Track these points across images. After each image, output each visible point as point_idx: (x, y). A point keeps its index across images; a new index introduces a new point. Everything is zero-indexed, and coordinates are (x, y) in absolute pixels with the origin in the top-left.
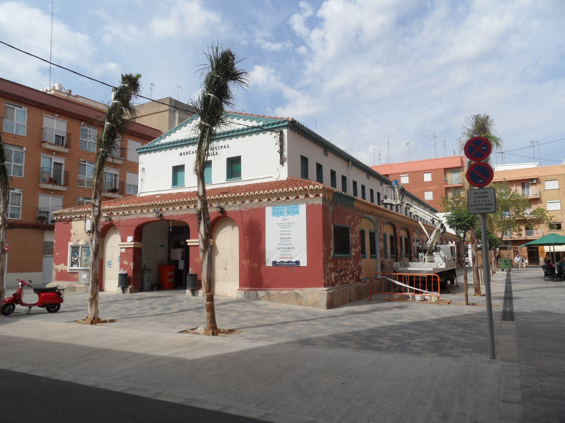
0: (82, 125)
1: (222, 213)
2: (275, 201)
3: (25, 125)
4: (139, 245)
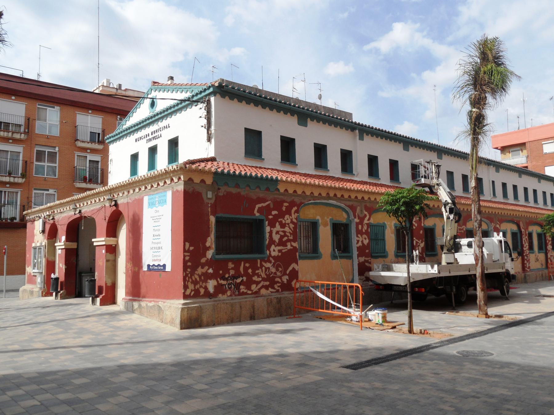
0: (118, 119)
1: (116, 207)
2: (150, 188)
3: (58, 125)
4: (73, 245)
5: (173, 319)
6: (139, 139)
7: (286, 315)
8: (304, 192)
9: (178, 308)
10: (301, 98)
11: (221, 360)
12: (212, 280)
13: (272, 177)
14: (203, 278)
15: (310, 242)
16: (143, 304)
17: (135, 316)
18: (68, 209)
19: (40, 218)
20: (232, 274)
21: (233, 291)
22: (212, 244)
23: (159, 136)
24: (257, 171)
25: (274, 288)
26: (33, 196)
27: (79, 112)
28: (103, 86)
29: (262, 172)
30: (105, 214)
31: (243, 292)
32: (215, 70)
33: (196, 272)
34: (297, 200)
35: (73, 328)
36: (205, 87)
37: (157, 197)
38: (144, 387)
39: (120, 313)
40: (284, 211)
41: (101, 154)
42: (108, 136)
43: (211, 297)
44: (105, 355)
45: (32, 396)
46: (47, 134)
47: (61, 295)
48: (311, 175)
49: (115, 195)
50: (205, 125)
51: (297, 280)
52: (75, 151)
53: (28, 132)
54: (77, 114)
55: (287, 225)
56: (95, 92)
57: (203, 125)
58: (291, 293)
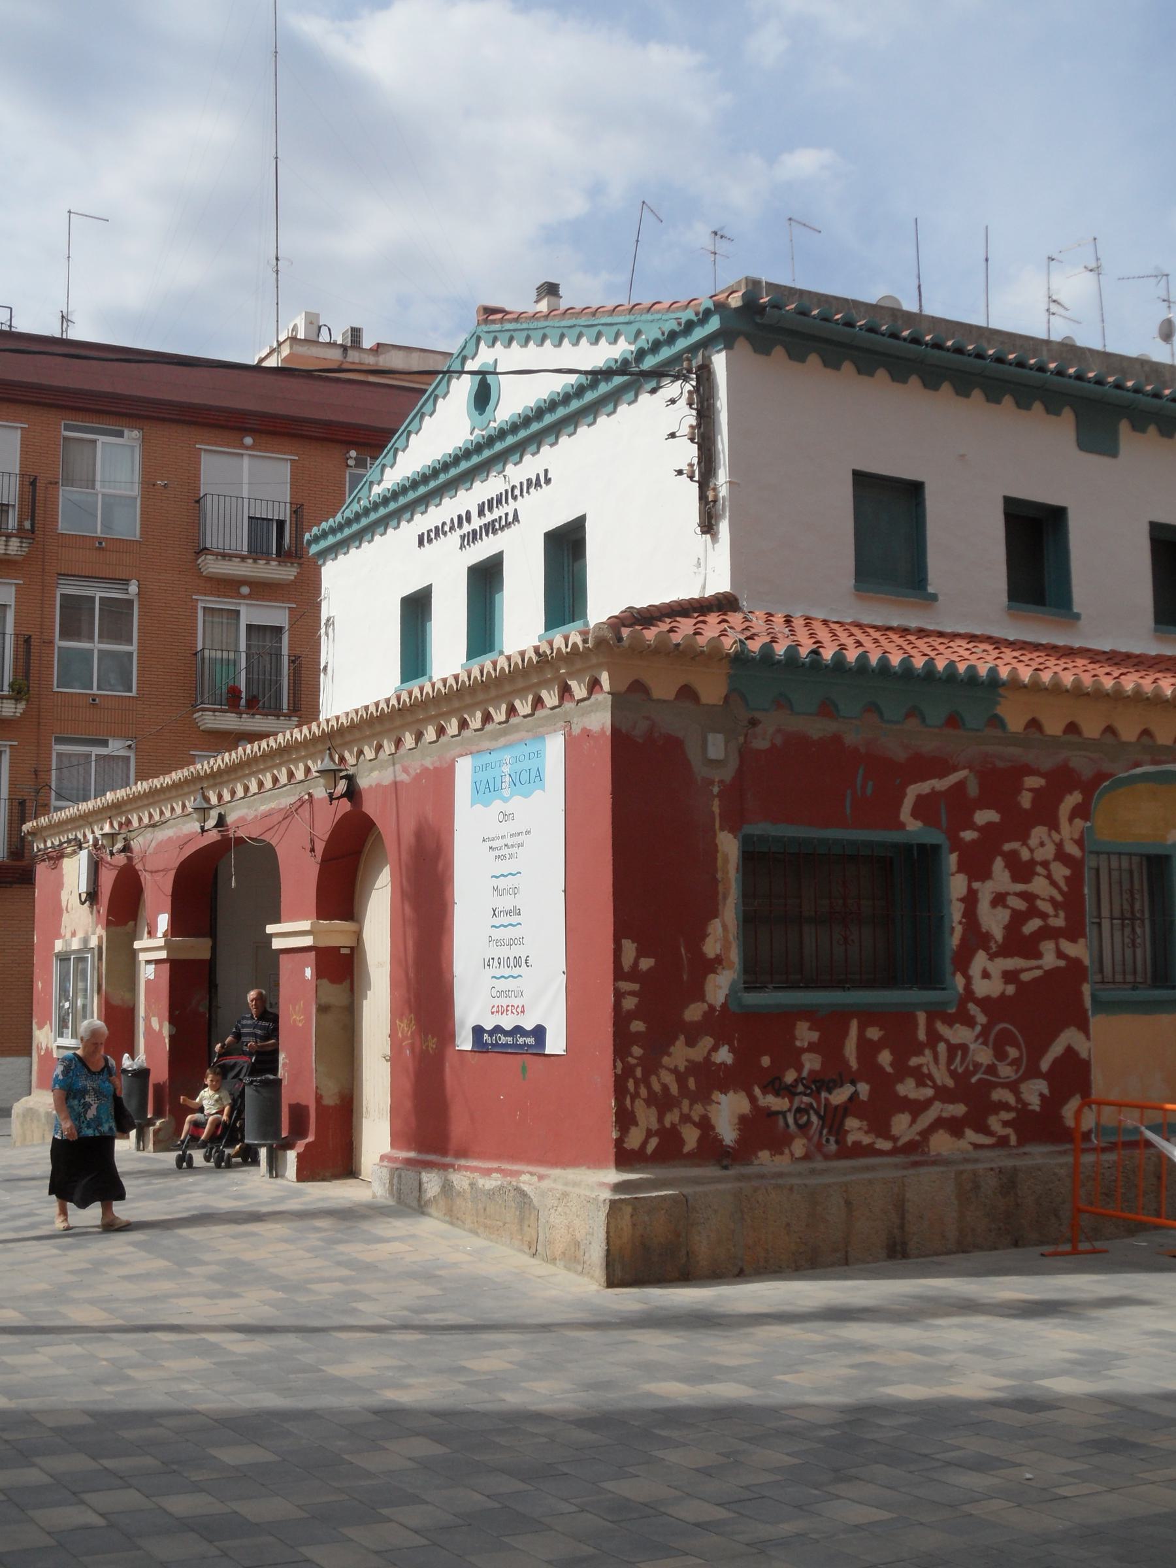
0: (351, 462)
4: (199, 948)
5: (577, 1244)
6: (432, 535)
7: (1041, 1243)
8: (1110, 730)
9: (596, 1199)
10: (1088, 339)
11: (773, 1412)
12: (731, 1094)
13: (972, 669)
14: (692, 1083)
15: (1138, 941)
16: (460, 1180)
17: (430, 1226)
18: (178, 810)
19: (81, 848)
20: (811, 1072)
21: (816, 1138)
22: (726, 946)
23: (510, 519)
24: (908, 648)
25: (984, 1129)
26: (54, 767)
27: (208, 444)
28: (293, 339)
29: (928, 651)
30: (312, 826)
31: (857, 1144)
32: (723, 246)
33: (666, 1060)
34: (1083, 764)
35: (206, 1257)
36: (689, 315)
37: (505, 761)
38: (477, 1497)
39: (373, 1211)
40: (1026, 811)
41: (289, 601)
42: (315, 530)
43: (725, 1163)
44: (323, 1368)
45: (74, 1494)
46: (99, 534)
47: (156, 1133)
48: (1138, 656)
49: (347, 755)
50: (691, 465)
51: (1087, 1100)
52: (198, 593)
53: (33, 531)
54: (203, 453)
55: (1039, 869)
56: (265, 364)
57: (685, 468)
58: (1060, 1153)
